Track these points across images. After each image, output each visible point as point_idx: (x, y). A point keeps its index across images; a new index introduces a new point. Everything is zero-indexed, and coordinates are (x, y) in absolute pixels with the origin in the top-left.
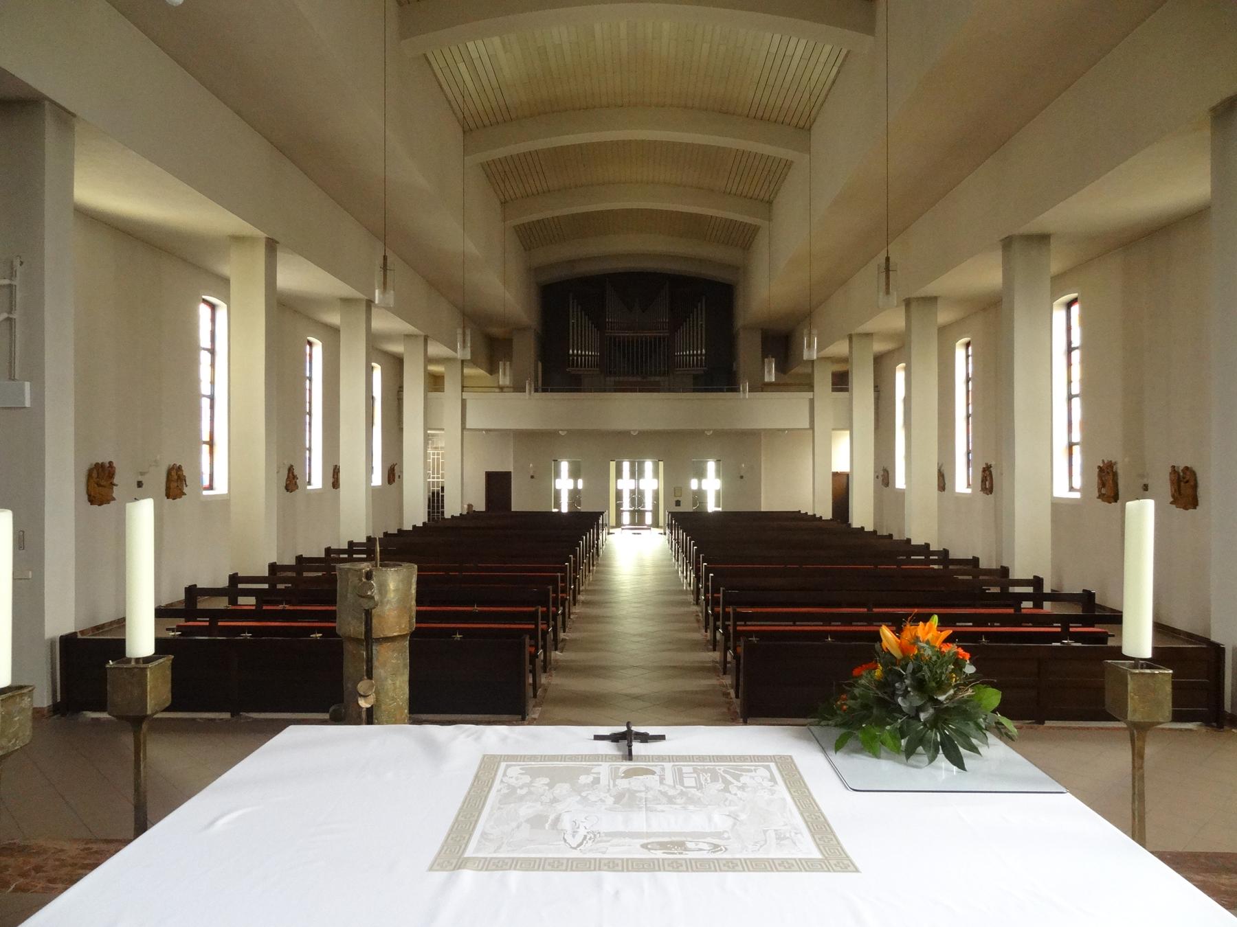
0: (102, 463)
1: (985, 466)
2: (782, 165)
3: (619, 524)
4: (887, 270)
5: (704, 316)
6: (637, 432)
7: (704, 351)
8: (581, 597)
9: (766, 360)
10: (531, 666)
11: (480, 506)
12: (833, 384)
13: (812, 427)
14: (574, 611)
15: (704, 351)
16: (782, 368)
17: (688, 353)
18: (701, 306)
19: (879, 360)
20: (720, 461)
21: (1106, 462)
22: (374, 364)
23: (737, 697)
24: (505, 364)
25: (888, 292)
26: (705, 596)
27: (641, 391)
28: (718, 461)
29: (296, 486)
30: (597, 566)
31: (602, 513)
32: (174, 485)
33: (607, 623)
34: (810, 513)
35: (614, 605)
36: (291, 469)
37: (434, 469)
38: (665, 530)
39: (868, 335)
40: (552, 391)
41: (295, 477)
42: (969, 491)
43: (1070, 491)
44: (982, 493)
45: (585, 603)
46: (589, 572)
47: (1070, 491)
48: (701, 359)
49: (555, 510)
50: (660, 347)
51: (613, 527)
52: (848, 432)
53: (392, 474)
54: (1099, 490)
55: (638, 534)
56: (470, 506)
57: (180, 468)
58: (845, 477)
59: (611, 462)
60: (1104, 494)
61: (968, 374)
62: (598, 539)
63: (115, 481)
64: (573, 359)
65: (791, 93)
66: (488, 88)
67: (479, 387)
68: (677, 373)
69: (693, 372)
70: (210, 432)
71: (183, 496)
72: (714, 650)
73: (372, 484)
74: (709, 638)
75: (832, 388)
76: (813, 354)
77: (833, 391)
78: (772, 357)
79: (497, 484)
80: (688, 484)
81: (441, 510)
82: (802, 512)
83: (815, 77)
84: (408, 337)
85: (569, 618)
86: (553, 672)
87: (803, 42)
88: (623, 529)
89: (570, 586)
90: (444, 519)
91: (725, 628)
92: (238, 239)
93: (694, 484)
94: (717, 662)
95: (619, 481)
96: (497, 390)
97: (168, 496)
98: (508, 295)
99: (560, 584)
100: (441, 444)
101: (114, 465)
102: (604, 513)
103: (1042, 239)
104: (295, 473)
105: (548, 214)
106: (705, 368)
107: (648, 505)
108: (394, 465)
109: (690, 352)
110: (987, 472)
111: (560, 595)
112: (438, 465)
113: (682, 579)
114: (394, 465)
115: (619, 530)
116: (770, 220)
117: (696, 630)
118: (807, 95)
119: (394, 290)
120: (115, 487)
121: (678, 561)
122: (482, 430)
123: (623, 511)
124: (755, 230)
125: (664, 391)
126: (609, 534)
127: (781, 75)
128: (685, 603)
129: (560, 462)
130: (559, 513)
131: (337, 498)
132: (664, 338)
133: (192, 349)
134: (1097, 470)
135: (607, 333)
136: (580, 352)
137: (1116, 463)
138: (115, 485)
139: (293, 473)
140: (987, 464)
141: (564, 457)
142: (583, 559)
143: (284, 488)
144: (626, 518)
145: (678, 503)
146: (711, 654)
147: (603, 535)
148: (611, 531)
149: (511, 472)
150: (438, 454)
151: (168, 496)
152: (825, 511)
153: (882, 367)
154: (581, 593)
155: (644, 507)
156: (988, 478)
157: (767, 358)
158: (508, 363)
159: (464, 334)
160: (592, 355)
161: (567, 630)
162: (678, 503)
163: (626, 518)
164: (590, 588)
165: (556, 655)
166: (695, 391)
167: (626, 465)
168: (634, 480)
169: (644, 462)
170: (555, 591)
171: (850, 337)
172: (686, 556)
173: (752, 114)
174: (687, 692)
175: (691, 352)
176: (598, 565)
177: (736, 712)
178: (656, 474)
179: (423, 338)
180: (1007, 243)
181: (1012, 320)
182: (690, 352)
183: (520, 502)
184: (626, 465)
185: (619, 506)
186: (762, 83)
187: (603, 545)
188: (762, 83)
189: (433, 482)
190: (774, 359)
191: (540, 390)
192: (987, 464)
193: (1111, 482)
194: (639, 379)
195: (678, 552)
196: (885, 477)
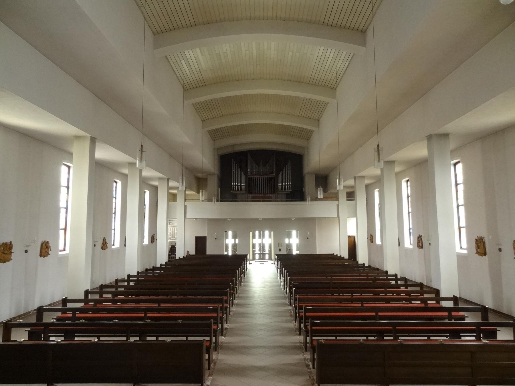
0: (6, 243)
1: (418, 236)
2: (324, 104)
3: (254, 259)
4: (378, 151)
5: (290, 169)
6: (262, 219)
7: (290, 183)
8: (236, 301)
9: (319, 188)
11: (193, 252)
12: (347, 197)
13: (338, 216)
14: (232, 310)
15: (290, 183)
16: (325, 191)
17: (283, 184)
18: (289, 164)
19: (367, 186)
20: (298, 231)
21: (479, 237)
22: (145, 190)
23: (314, 368)
25: (379, 161)
27: (264, 201)
28: (297, 231)
29: (106, 247)
30: (244, 283)
31: (247, 255)
32: (44, 251)
34: (339, 255)
35: (251, 306)
36: (104, 239)
37: (172, 235)
38: (274, 262)
39: (363, 177)
40: (224, 201)
41: (106, 243)
42: (411, 247)
43: (460, 249)
44: (418, 248)
45: (238, 305)
46: (240, 286)
47: (460, 249)
48: (289, 187)
49: (225, 253)
50: (271, 182)
51: (251, 260)
52: (355, 218)
53: (153, 239)
54: (476, 250)
55: (262, 264)
56: (188, 252)
57: (47, 242)
58: (353, 238)
59: (250, 232)
60: (479, 252)
61: (408, 194)
62: (244, 269)
63: (13, 251)
64: (234, 187)
65: (328, 73)
66: (195, 72)
67: (193, 200)
68: (279, 193)
69: (285, 192)
70: (65, 224)
71: (49, 256)
72: (300, 335)
73: (144, 244)
74: (297, 327)
75: (347, 199)
77: (347, 201)
79: (200, 242)
80: (284, 241)
81: (175, 254)
83: (339, 66)
84: (160, 179)
85: (230, 314)
86: (220, 351)
87: (333, 50)
88: (256, 262)
89: (230, 298)
90: (176, 260)
92: (77, 137)
93: (287, 241)
94: (301, 343)
95: (254, 239)
97: (41, 256)
100: (175, 224)
101: (13, 243)
103: (446, 135)
104: (106, 241)
105: (224, 125)
106: (291, 191)
107: (267, 251)
108: (154, 235)
109: (284, 184)
110: (420, 239)
111: (225, 305)
112: (174, 233)
114: (154, 235)
115: (254, 261)
116: (318, 127)
117: (291, 322)
118: (335, 74)
119: (146, 161)
120: (12, 254)
121: (280, 279)
122: (194, 218)
123: (256, 254)
124: (312, 132)
126: (249, 264)
127: (324, 65)
128: (284, 305)
130: (227, 255)
131: (124, 250)
132: (273, 178)
133: (57, 187)
134: (475, 241)
135: (248, 175)
136: (236, 184)
137: (484, 238)
138: (12, 253)
139: (105, 241)
140: (419, 235)
142: (237, 282)
143: (101, 249)
144: (257, 257)
145: (280, 250)
146: (298, 337)
148: (251, 262)
149: (206, 237)
150: (174, 229)
151: (41, 256)
152: (345, 255)
153: (369, 189)
154: (236, 299)
155: (265, 252)
156: (420, 241)
157: (319, 187)
159: (182, 179)
160: (242, 185)
161: (228, 322)
162: (280, 250)
163: (257, 257)
164: (240, 295)
165: (222, 339)
166: (287, 201)
167: (257, 233)
168: (260, 239)
171: (355, 178)
172: (284, 279)
173: (311, 82)
174: (289, 364)
175: (285, 184)
176: (245, 282)
177: (314, 379)
178: (270, 237)
179: (167, 180)
180: (429, 138)
181: (434, 172)
182: (284, 184)
183: (210, 250)
184: (257, 233)
185: (254, 251)
186: (315, 69)
187: (247, 270)
188: (315, 69)
189: (172, 241)
190: (322, 188)
191: (219, 201)
192: (419, 235)
193: (482, 246)
194: (263, 195)
195: (281, 275)
196: (371, 239)
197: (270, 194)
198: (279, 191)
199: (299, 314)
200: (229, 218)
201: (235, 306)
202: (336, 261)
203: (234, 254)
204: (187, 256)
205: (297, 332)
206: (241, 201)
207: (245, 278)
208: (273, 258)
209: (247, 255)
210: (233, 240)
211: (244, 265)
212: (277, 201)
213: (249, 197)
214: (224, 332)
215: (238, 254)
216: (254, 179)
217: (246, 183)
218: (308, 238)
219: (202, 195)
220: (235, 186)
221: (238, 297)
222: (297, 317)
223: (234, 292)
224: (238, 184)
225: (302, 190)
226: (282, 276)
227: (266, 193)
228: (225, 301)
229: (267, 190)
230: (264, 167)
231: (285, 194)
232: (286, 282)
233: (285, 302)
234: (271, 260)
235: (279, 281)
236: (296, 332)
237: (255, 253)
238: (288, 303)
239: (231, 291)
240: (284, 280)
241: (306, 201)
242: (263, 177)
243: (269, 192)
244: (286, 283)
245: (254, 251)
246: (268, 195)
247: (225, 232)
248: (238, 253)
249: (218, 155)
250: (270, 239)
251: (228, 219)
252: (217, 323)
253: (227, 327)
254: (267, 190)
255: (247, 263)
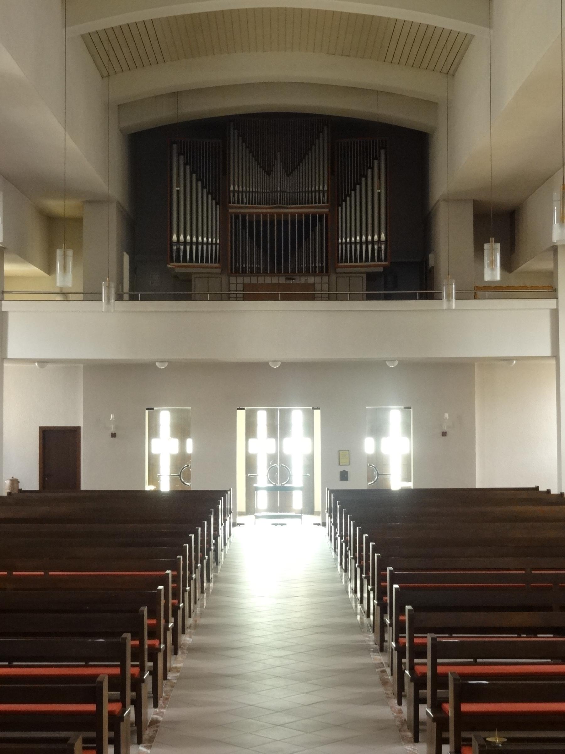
3: (250, 510)
6: (279, 364)
8: (186, 639)
9: (486, 246)
10: (134, 694)
13: (556, 355)
20: (410, 408)
24: (65, 255)
26: (397, 642)
27: (286, 298)
28: (405, 408)
31: (223, 493)
33: (231, 687)
34: (554, 491)
38: (324, 518)
40: (145, 298)
45: (194, 650)
46: (202, 592)
48: (380, 249)
49: (149, 488)
51: (241, 514)
55: (282, 525)
59: (238, 411)
62: (216, 537)
64: (178, 250)
69: (363, 270)
72: (416, 740)
76: (452, 305)
78: (496, 241)
82: (541, 489)
85: (165, 678)
88: (257, 517)
89: (167, 622)
91: (437, 706)
95: (251, 440)
96: (59, 297)
98: (71, 143)
99: (147, 621)
102: (226, 492)
106: (383, 263)
111: (147, 642)
113: (354, 604)
115: (251, 517)
117: (382, 701)
121: (346, 570)
122: (32, 361)
123: (257, 489)
125: (322, 298)
126: (235, 525)
128: (363, 649)
129: (158, 411)
130: (156, 494)
136: (188, 238)
141: (164, 403)
142: (191, 573)
145: (344, 476)
147: (225, 527)
148: (239, 520)
154: (187, 631)
158: (70, 253)
161: (161, 702)
162: (344, 476)
164: (202, 621)
166: (370, 297)
167: (262, 416)
168: (273, 440)
169: (289, 411)
170: (153, 614)
175: (364, 237)
184: (262, 416)
185: (250, 481)
187: (225, 544)
191: (126, 297)
194: (282, 280)
195: (347, 557)
197: (308, 273)
198: (340, 264)
199: (412, 669)
200: (162, 361)
201: (183, 653)
202: (546, 508)
203: (180, 489)
204: (9, 494)
205: (403, 734)
206: (203, 298)
207: (220, 567)
208: (318, 506)
209: (226, 492)
210: (176, 442)
211: (216, 520)
212: (337, 298)
213: (233, 287)
214: (147, 732)
215: (192, 489)
216: (251, 223)
217: (223, 237)
218: (444, 434)
219: (64, 268)
220: (182, 247)
221: (196, 626)
222: (406, 680)
223: (181, 605)
224: (194, 239)
225: (426, 261)
226: (350, 556)
227: (293, 271)
228: (149, 633)
229: (300, 262)
230: (288, 176)
231: (364, 276)
232: (367, 573)
233: (364, 641)
234: (311, 511)
235: (342, 576)
236: (400, 731)
237: (255, 485)
238: (372, 643)
239: (171, 601)
240: (359, 570)
241: (440, 298)
242: (286, 215)
243: (307, 268)
244: (367, 578)
245: (250, 481)
246: (303, 280)
247: (147, 411)
248: (193, 485)
249: (121, 131)
250: (309, 440)
251: (157, 363)
252: (122, 700)
253: (155, 716)
254: (300, 262)
255: (228, 518)
